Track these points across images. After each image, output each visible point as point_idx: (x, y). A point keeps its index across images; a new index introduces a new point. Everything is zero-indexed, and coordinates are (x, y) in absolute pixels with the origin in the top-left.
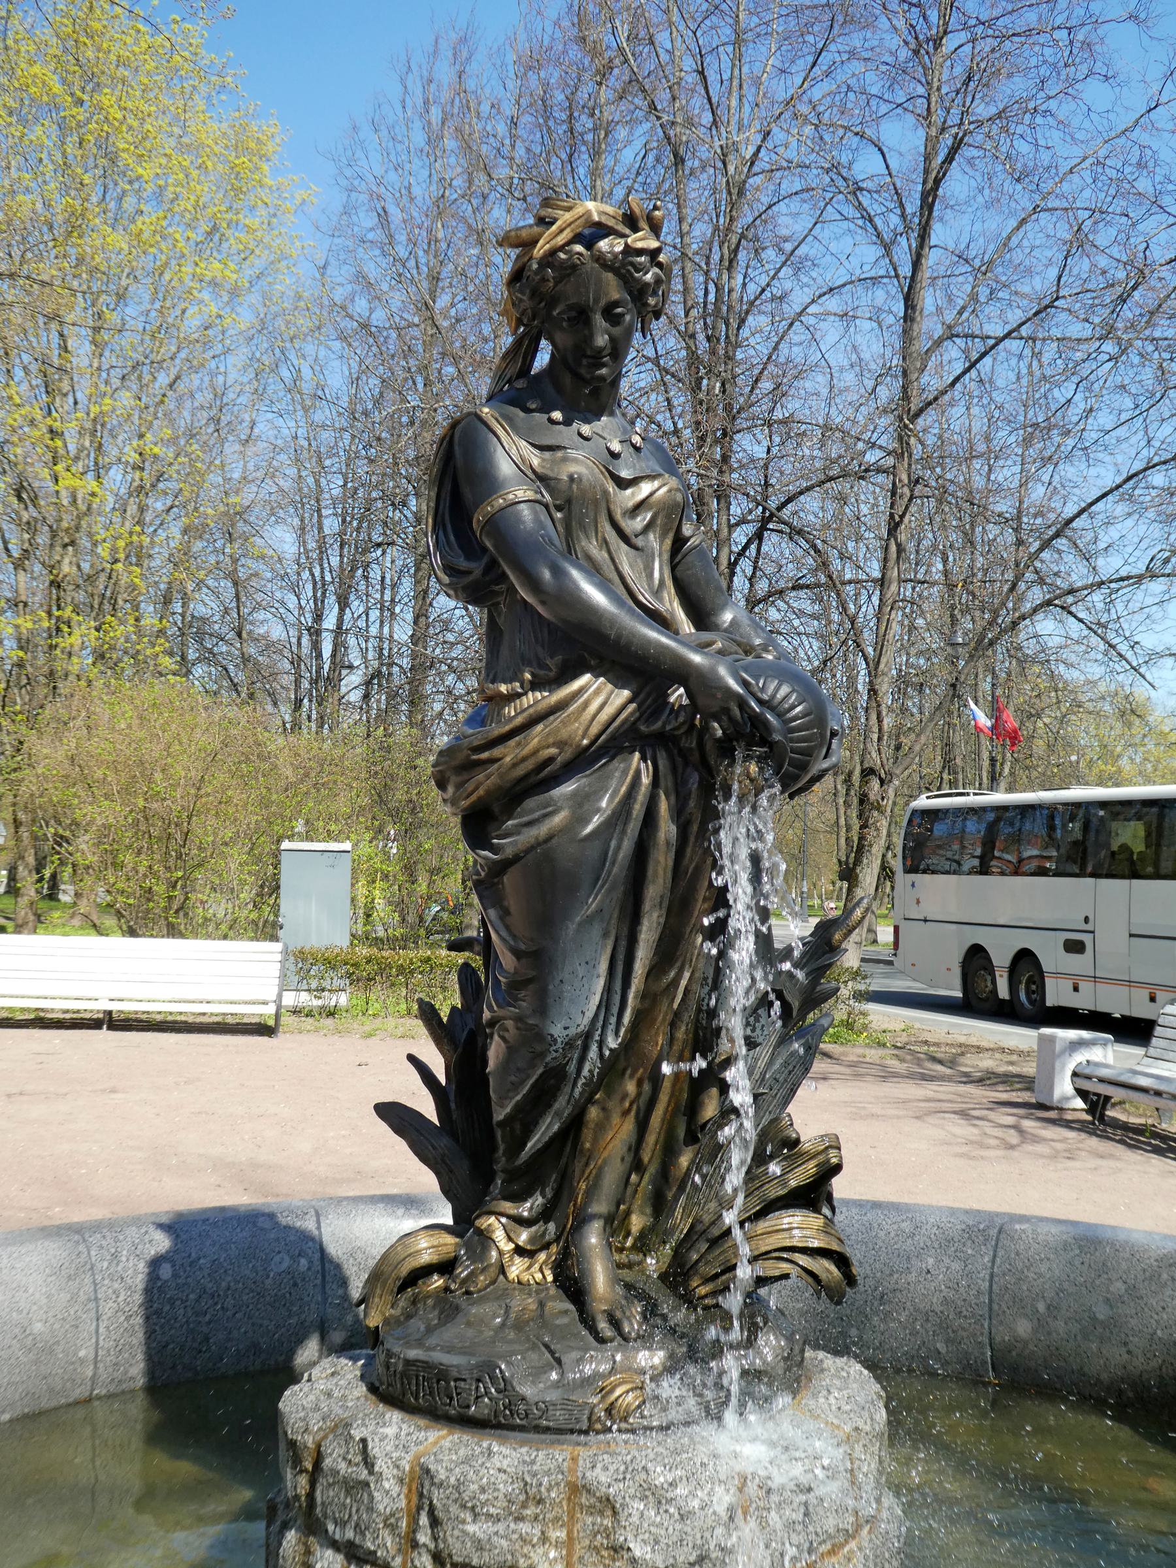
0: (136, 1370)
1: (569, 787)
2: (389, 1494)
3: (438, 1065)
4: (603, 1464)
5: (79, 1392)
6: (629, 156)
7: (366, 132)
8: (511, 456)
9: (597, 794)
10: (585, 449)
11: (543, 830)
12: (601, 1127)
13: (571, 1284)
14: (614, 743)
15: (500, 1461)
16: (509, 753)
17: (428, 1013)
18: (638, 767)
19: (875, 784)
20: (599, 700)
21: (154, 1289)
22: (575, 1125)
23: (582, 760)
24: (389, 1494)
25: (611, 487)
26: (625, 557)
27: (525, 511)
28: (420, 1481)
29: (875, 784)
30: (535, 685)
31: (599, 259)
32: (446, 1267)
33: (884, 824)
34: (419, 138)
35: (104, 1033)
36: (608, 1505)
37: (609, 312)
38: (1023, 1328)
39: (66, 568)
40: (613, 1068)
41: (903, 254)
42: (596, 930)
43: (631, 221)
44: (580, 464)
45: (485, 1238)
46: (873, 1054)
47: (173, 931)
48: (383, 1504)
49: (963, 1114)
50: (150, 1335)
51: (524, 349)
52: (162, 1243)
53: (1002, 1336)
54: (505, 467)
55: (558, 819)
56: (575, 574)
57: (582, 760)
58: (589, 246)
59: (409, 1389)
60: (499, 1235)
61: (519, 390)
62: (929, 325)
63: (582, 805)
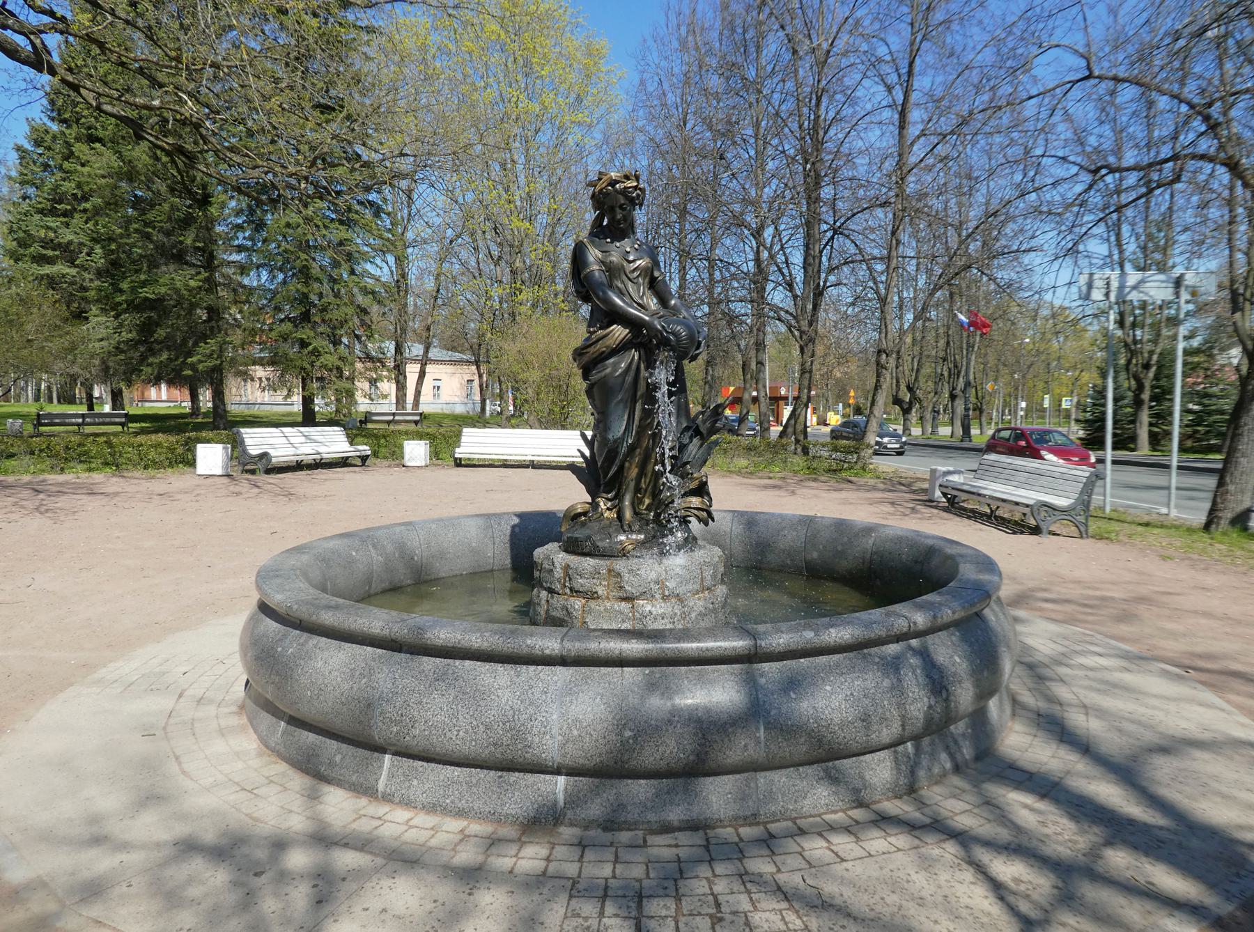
0: (508, 562)
1: (611, 360)
2: (558, 573)
3: (587, 453)
4: (620, 565)
5: (489, 567)
6: (773, 48)
7: (650, 42)
8: (593, 254)
9: (620, 363)
10: (617, 251)
11: (603, 374)
12: (629, 469)
13: (620, 517)
14: (623, 347)
15: (590, 562)
16: (592, 350)
17: (584, 436)
18: (635, 354)
19: (884, 356)
20: (619, 332)
21: (513, 535)
22: (621, 468)
23: (615, 352)
24: (558, 573)
25: (625, 264)
26: (630, 286)
27: (597, 273)
28: (567, 568)
29: (884, 356)
30: (601, 328)
31: (616, 191)
32: (585, 514)
33: (888, 376)
34: (676, 44)
35: (530, 470)
36: (619, 575)
37: (621, 207)
38: (815, 555)
39: (517, 264)
40: (632, 449)
41: (899, 96)
42: (621, 406)
43: (627, 177)
44: (615, 258)
45: (597, 505)
46: (872, 482)
47: (563, 427)
48: (556, 575)
49: (893, 503)
50: (512, 549)
51: (599, 220)
52: (516, 520)
53: (809, 557)
54: (591, 259)
55: (608, 370)
56: (611, 294)
57: (615, 352)
58: (613, 186)
59: (572, 547)
60: (602, 504)
61: (600, 232)
62: (913, 131)
63: (616, 365)
